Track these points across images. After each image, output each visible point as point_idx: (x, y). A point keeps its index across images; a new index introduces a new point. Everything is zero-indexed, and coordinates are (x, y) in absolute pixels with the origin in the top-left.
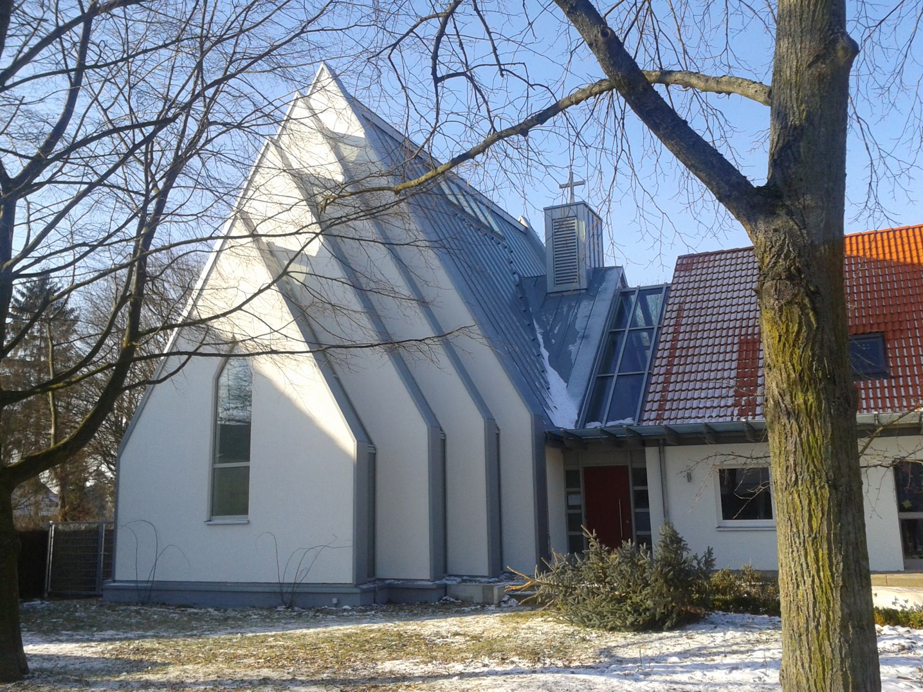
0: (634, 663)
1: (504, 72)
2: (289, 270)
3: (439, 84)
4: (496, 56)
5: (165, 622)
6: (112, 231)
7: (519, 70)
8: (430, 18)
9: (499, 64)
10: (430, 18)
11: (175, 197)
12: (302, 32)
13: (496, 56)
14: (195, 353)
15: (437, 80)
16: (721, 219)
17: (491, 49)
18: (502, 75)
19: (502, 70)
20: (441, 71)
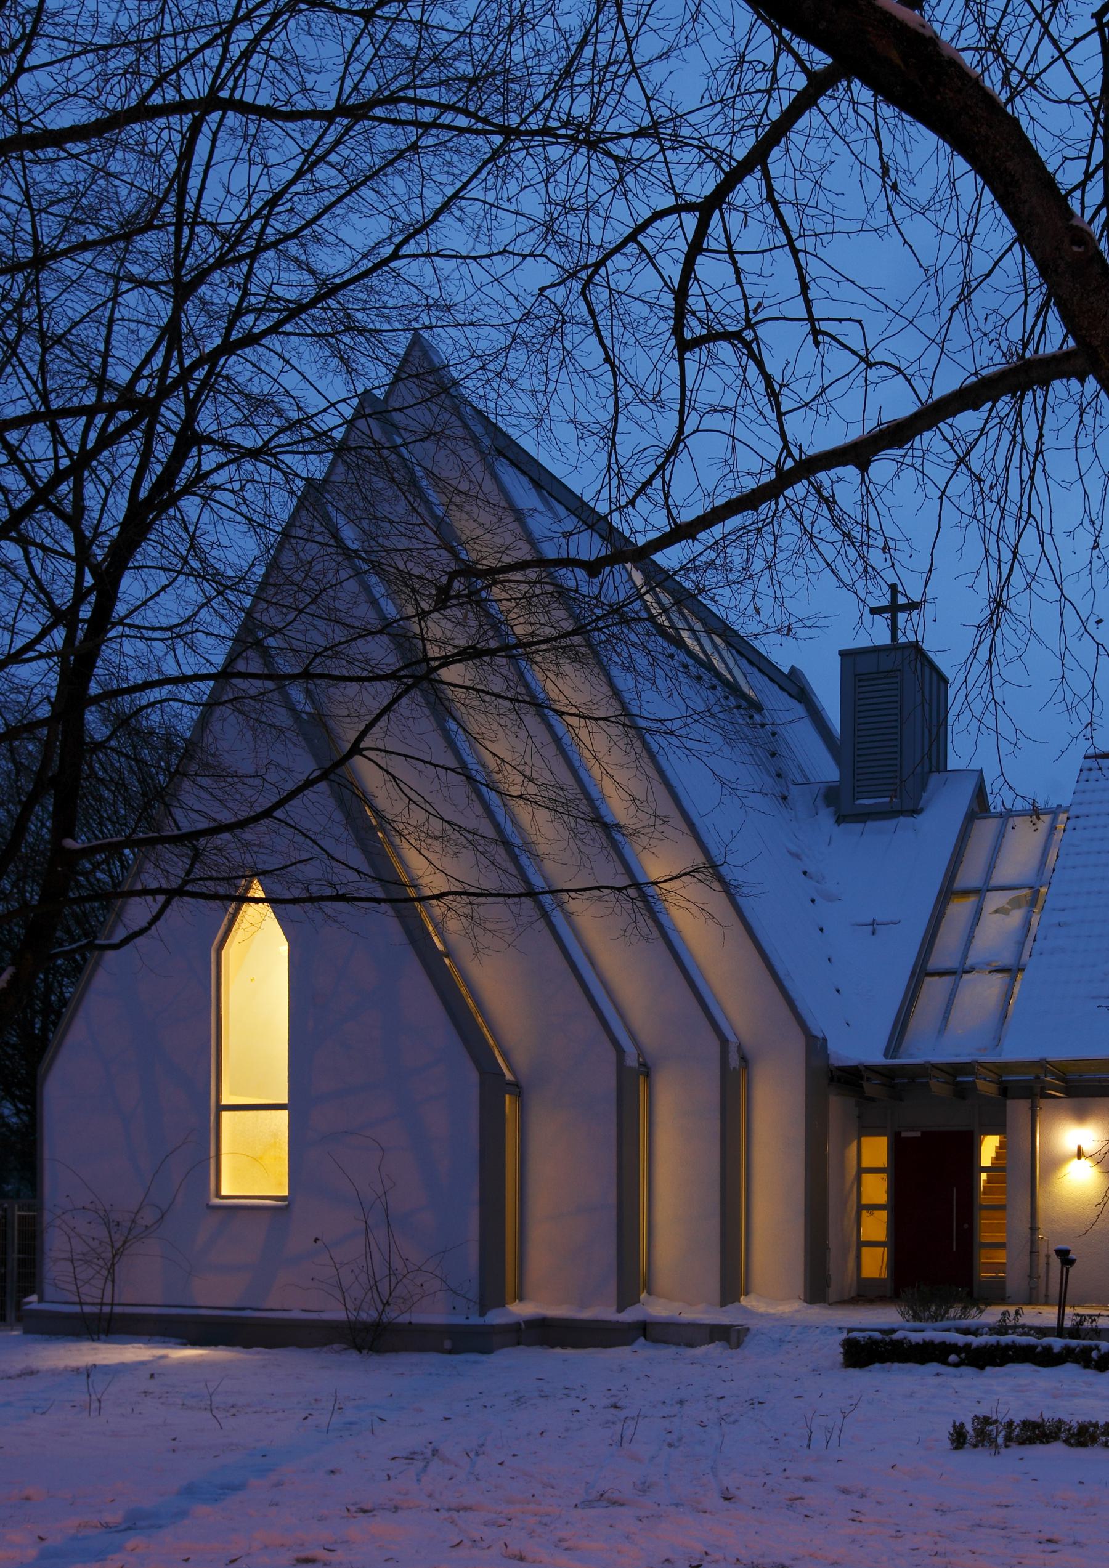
0: (1048, 1349)
1: (820, 338)
2: (362, 745)
3: (688, 355)
4: (808, 303)
5: (158, 1342)
6: (300, 456)
7: (852, 335)
8: (822, 113)
9: (811, 319)
10: (822, 113)
11: (131, 587)
12: (395, 256)
13: (808, 303)
14: (180, 892)
15: (684, 347)
16: (869, 115)
17: (798, 289)
18: (817, 344)
19: (815, 332)
20: (694, 329)
